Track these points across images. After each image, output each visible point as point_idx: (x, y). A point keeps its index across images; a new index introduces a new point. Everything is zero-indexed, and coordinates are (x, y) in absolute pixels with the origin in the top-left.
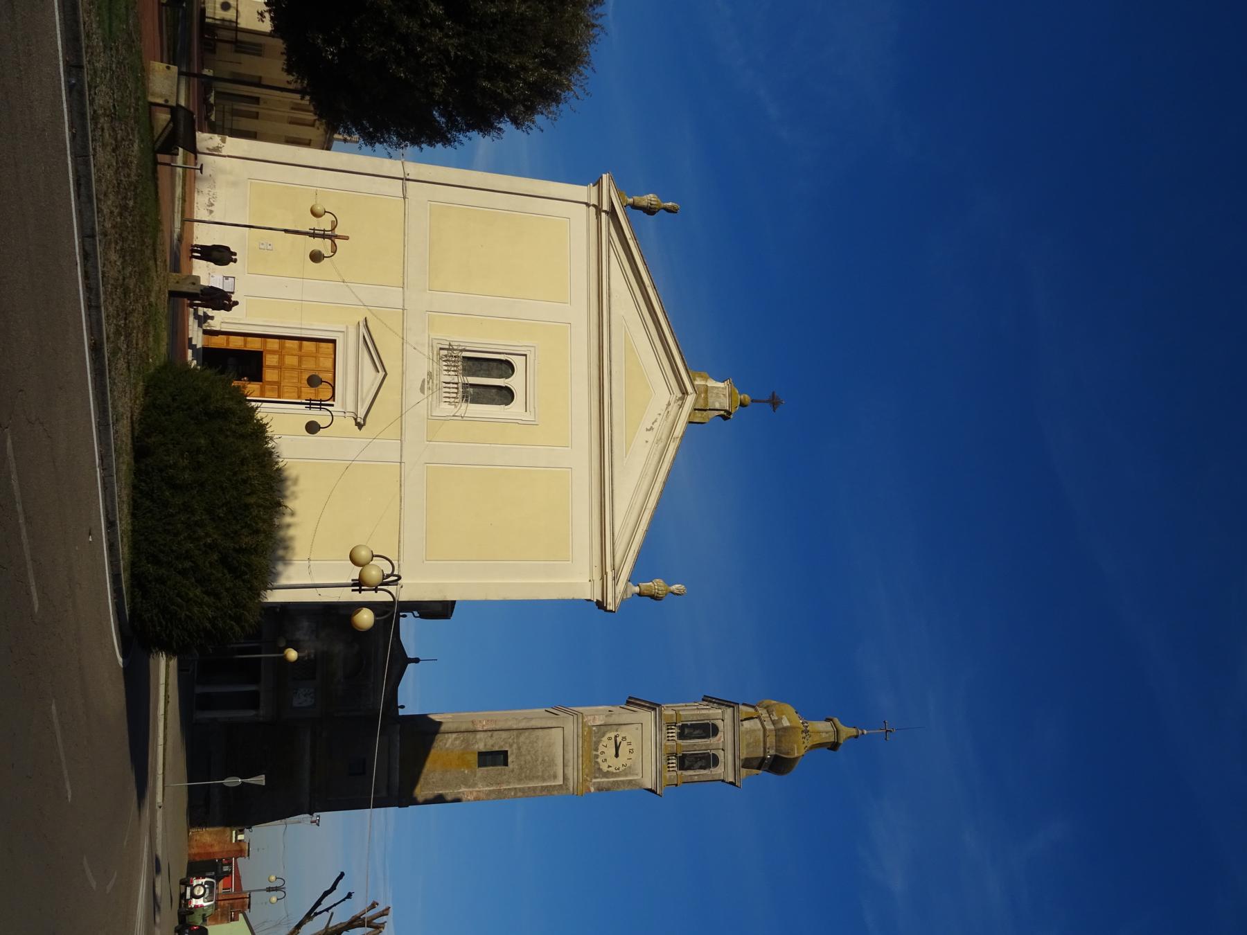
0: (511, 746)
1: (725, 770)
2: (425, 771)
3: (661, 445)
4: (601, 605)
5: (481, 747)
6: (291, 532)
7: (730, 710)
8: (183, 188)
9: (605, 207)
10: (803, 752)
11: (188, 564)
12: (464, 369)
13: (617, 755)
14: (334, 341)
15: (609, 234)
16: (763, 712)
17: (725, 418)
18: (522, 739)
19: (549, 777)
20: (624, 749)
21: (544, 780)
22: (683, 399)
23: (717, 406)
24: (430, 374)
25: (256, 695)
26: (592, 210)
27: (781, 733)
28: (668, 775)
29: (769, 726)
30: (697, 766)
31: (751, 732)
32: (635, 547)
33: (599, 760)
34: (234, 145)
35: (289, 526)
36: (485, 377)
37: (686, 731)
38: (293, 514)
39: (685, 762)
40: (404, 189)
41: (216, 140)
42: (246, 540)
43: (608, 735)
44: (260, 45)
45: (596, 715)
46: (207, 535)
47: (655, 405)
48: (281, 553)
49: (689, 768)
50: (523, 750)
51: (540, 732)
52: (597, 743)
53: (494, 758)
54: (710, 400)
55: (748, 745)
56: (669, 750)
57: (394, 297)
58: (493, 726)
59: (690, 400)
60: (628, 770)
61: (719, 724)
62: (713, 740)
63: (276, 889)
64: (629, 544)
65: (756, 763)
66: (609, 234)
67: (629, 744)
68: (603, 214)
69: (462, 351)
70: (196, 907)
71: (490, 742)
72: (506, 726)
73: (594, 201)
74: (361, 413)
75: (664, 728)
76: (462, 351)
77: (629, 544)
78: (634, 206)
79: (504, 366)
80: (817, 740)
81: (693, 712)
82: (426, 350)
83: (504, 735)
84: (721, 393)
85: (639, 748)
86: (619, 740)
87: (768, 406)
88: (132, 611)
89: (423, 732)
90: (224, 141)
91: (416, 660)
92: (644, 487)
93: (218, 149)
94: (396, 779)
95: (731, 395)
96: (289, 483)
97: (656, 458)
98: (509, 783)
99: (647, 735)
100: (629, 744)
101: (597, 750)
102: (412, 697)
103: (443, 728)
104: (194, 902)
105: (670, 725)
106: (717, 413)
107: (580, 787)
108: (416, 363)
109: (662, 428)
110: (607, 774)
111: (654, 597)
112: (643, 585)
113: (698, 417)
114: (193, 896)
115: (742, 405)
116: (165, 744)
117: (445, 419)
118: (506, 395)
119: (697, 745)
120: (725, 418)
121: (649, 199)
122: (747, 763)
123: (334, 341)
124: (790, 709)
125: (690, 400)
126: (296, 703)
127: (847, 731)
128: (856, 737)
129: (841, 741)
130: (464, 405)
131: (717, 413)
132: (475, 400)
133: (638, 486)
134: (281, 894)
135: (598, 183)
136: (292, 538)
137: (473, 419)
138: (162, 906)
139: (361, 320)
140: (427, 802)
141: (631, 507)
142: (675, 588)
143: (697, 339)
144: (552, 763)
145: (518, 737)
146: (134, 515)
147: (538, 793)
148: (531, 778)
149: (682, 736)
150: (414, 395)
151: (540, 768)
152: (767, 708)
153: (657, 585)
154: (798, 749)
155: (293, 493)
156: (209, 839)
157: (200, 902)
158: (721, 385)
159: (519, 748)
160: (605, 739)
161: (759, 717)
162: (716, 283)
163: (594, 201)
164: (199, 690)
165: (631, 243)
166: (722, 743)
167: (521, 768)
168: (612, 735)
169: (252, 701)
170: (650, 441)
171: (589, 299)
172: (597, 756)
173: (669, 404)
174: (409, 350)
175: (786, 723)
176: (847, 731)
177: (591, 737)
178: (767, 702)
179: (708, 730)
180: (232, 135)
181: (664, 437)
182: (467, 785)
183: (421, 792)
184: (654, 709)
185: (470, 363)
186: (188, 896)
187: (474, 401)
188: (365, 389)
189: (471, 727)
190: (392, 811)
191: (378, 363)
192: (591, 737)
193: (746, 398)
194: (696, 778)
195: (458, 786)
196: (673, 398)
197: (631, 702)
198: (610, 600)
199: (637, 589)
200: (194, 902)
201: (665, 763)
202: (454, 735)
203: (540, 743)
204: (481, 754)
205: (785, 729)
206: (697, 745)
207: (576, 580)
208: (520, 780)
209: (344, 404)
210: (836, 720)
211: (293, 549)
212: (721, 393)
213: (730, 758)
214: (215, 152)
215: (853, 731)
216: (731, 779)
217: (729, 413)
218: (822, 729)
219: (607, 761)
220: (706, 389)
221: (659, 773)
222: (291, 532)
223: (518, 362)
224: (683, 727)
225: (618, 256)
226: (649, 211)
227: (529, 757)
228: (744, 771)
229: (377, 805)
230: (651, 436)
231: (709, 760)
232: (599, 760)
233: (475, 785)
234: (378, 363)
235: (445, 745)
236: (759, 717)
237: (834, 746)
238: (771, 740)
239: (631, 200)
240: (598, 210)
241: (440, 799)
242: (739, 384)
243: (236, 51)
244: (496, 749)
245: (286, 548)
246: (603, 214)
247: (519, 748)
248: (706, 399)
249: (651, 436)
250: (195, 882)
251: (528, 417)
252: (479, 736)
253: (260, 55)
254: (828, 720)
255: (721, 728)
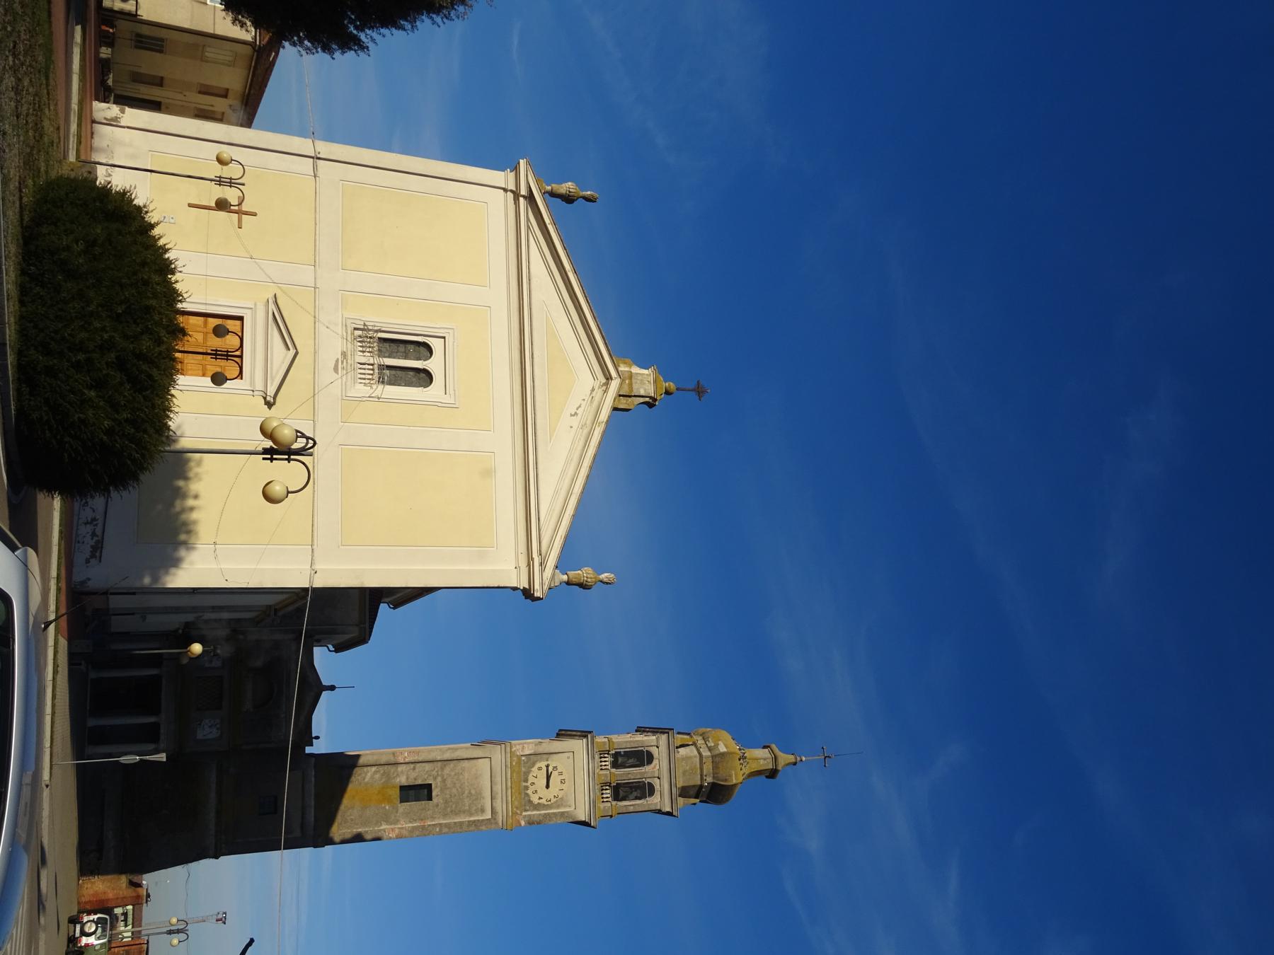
0: (435, 779)
1: (660, 800)
2: (342, 807)
3: (586, 431)
4: (527, 593)
5: (403, 781)
6: (194, 516)
7: (664, 737)
8: (79, 125)
9: (523, 192)
10: (741, 779)
11: (81, 357)
12: (379, 350)
13: (548, 787)
14: (241, 319)
15: (528, 220)
16: (700, 742)
17: (650, 405)
18: (447, 771)
19: (476, 811)
20: (555, 779)
21: (471, 815)
22: (607, 384)
23: (642, 392)
24: (344, 354)
25: (156, 726)
26: (510, 195)
27: (718, 759)
28: (602, 806)
29: (706, 753)
30: (632, 796)
31: (687, 758)
32: (562, 532)
33: (529, 792)
34: (134, 116)
35: (192, 509)
36: (402, 359)
37: (620, 760)
38: (196, 497)
39: (620, 791)
40: (315, 168)
41: (114, 110)
42: (146, 344)
43: (538, 765)
44: (162, 40)
45: (527, 747)
46: (103, 329)
47: (579, 391)
48: (183, 537)
49: (624, 799)
50: (449, 783)
51: (466, 764)
52: (527, 773)
53: (417, 792)
54: (635, 386)
55: (684, 772)
56: (603, 779)
57: (307, 275)
58: (416, 758)
59: (615, 384)
60: (560, 802)
61: (654, 750)
62: (647, 768)
63: (178, 931)
64: (556, 530)
65: (692, 792)
66: (528, 220)
67: (561, 774)
68: (521, 199)
69: (377, 331)
70: (87, 945)
71: (413, 775)
72: (430, 757)
73: (512, 186)
74: (271, 392)
75: (597, 757)
76: (377, 331)
77: (556, 530)
78: (553, 194)
79: (422, 349)
80: (755, 767)
81: (626, 740)
82: (339, 330)
83: (427, 767)
84: (646, 381)
85: (570, 779)
86: (550, 769)
87: (693, 395)
88: (19, 410)
89: (340, 768)
90: (123, 112)
91: (332, 688)
92: (570, 472)
93: (116, 119)
94: (311, 817)
95: (655, 382)
96: (192, 464)
97: (581, 443)
98: (433, 818)
99: (579, 764)
100: (561, 774)
101: (526, 781)
102: (329, 730)
103: (361, 761)
104: (84, 940)
105: (603, 753)
106: (642, 400)
107: (510, 821)
108: (328, 342)
109: (586, 414)
110: (538, 807)
111: (583, 586)
112: (571, 573)
113: (623, 404)
114: (83, 933)
115: (667, 393)
116: (53, 714)
117: (360, 400)
118: (425, 377)
119: (631, 774)
120: (650, 405)
121: (567, 187)
122: (684, 792)
123: (241, 319)
124: (726, 736)
125: (615, 384)
126: (200, 736)
127: (785, 758)
128: (795, 764)
129: (780, 768)
130: (381, 387)
131: (642, 400)
132: (392, 382)
133: (563, 472)
134: (182, 936)
135: (516, 169)
136: (195, 522)
137: (390, 401)
138: (47, 905)
139: (271, 296)
140: (344, 842)
141: (556, 492)
142: (604, 576)
143: (625, 312)
144: (479, 796)
145: (442, 769)
146: (22, 303)
147: (465, 827)
148: (456, 813)
149: (615, 765)
150: (327, 375)
151: (467, 802)
152: (702, 735)
153: (586, 573)
154: (736, 776)
155: (197, 474)
156: (99, 886)
157: (92, 940)
158: (646, 372)
159: (444, 781)
160: (535, 769)
161: (694, 744)
162: (642, 262)
163: (512, 186)
164: (92, 722)
165: (551, 228)
166: (656, 773)
167: (446, 802)
168: (543, 764)
169: (150, 736)
170: (575, 425)
171: (508, 283)
172: (527, 788)
173: (593, 390)
174: (321, 329)
175: (722, 749)
176: (785, 758)
177: (520, 769)
178: (703, 730)
179: (642, 757)
180: (131, 106)
181: (589, 422)
182: (388, 822)
183: (337, 831)
184: (586, 736)
185: (387, 345)
186: (78, 934)
187: (391, 383)
188: (275, 368)
189: (392, 760)
190: (307, 852)
191: (288, 341)
192: (520, 769)
193: (672, 386)
194: (631, 809)
195: (378, 823)
196: (597, 384)
197: (561, 734)
198: (537, 586)
199: (565, 578)
200: (84, 940)
201: (598, 794)
202: (374, 769)
203: (466, 775)
204: (402, 788)
205: (723, 754)
206: (631, 774)
207: (503, 567)
208: (445, 816)
209: (252, 382)
210: (773, 746)
211: (196, 533)
212: (646, 381)
213: (666, 786)
214: (113, 122)
215: (791, 758)
216: (668, 809)
217: (655, 400)
218: (760, 757)
219: (539, 792)
220: (631, 376)
221: (593, 804)
222: (194, 516)
223: (436, 344)
224: (616, 755)
225: (537, 242)
226: (568, 199)
227: (454, 791)
228: (681, 800)
229: (288, 846)
230: (575, 422)
231: (644, 790)
232: (529, 792)
233: (397, 822)
234: (288, 341)
235: (364, 779)
236: (694, 744)
237: (772, 774)
238: (708, 767)
239: (549, 188)
240: (516, 195)
241: (358, 838)
242: (664, 372)
243: (136, 47)
244: (419, 782)
245: (189, 532)
246: (521, 199)
247: (444, 781)
248: (631, 385)
249: (575, 422)
250: (85, 919)
251: (447, 399)
252: (400, 768)
253: (161, 51)
254: (765, 747)
255: (657, 787)
